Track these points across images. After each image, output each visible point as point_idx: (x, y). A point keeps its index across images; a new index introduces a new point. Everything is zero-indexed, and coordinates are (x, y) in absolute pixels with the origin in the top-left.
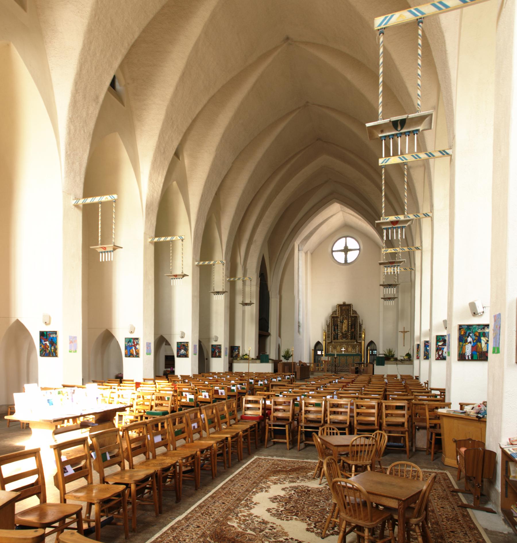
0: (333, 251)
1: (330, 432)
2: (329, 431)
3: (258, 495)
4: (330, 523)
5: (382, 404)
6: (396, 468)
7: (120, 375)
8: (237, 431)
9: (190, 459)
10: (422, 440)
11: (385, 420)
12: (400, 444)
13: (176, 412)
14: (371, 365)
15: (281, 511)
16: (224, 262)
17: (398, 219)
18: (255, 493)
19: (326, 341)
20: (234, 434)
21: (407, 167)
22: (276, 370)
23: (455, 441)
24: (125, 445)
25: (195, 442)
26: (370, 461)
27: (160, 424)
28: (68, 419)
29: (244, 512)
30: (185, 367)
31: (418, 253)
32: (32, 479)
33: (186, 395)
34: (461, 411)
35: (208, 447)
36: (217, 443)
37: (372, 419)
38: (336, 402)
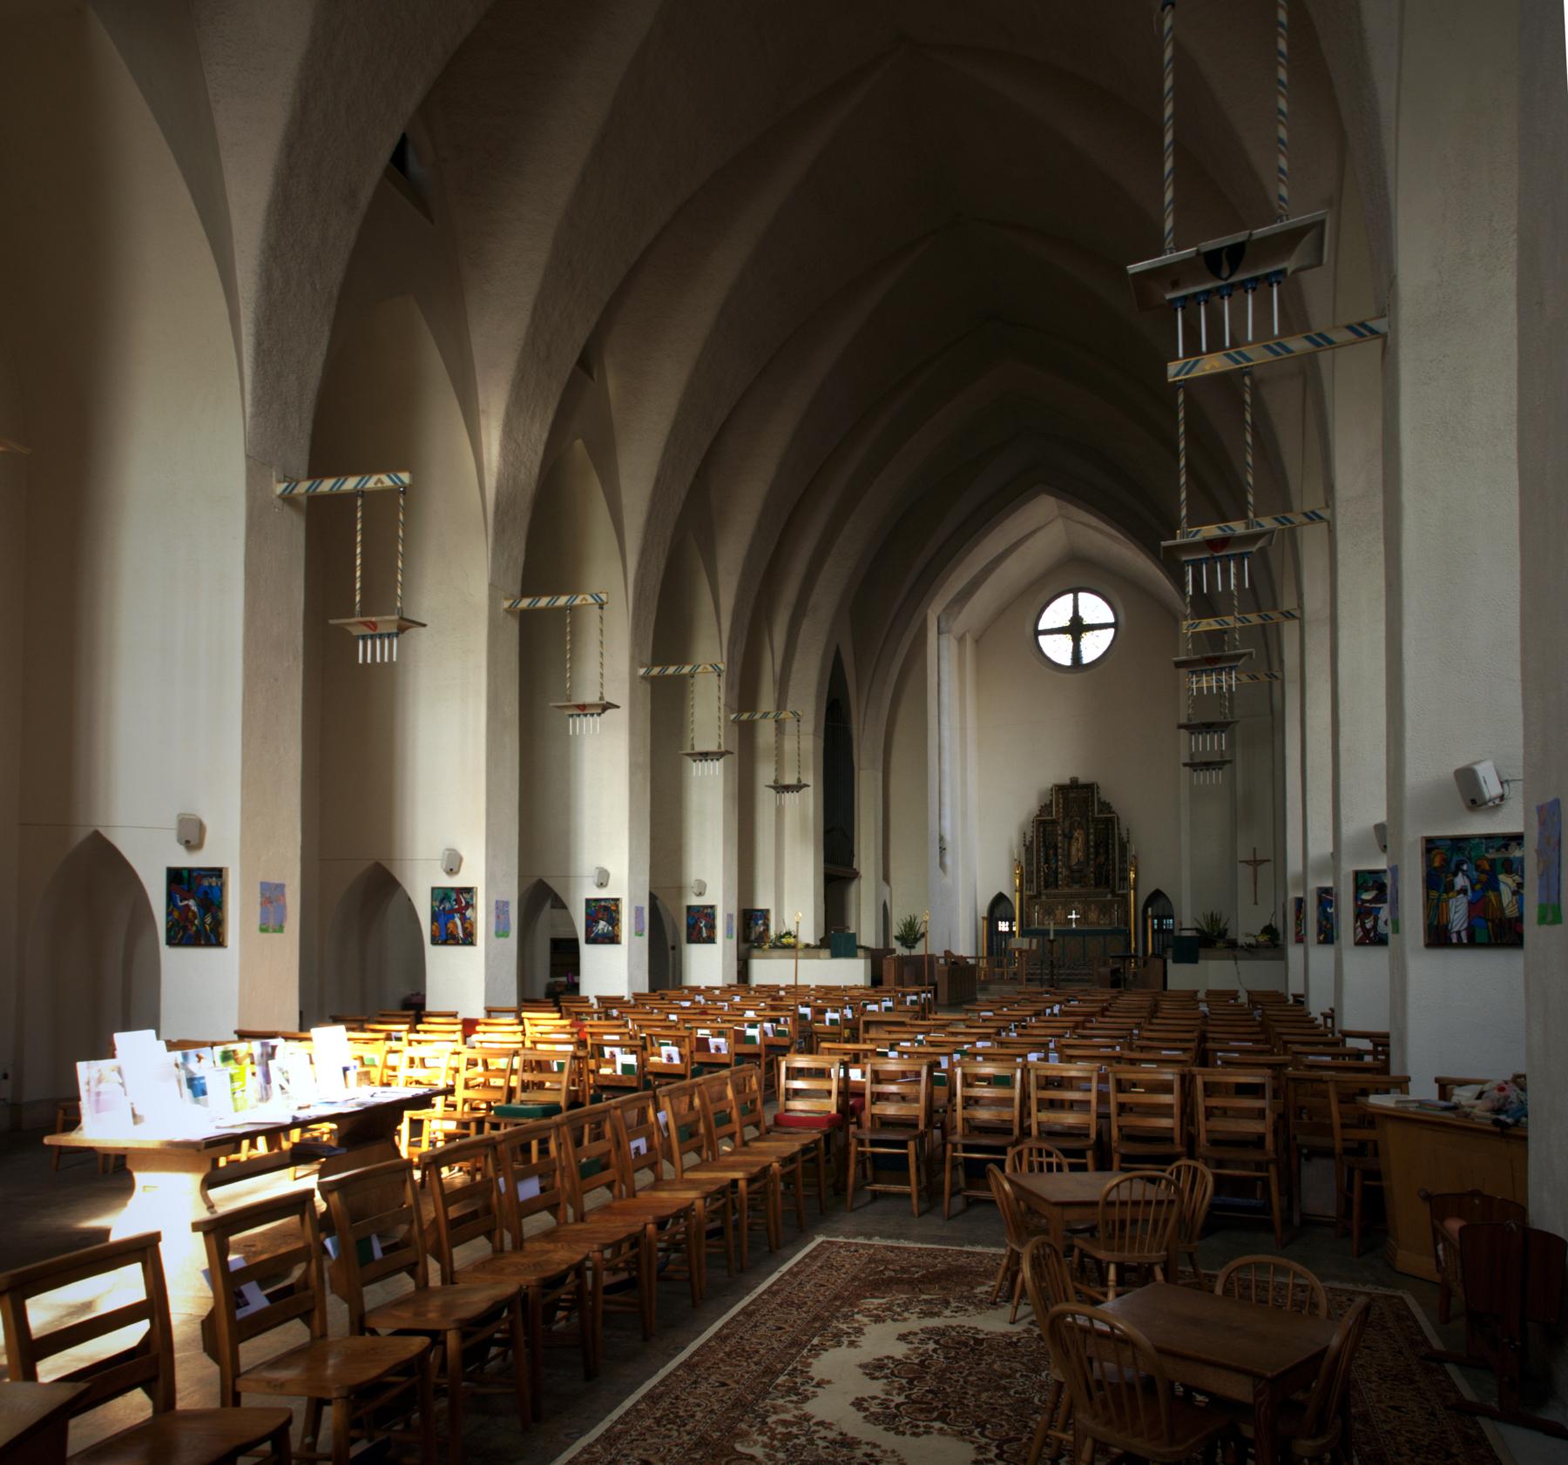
0: (1038, 633)
1: (1041, 1164)
2: (1035, 1159)
3: (826, 1357)
4: (1045, 1444)
5: (1193, 1077)
6: (1241, 1275)
7: (415, 1000)
8: (765, 1160)
9: (625, 1247)
10: (1320, 1189)
11: (1203, 1126)
12: (1254, 1202)
13: (582, 1105)
14: (1159, 963)
15: (898, 1406)
16: (722, 667)
17: (1229, 532)
18: (816, 1351)
19: (1021, 892)
20: (756, 1170)
21: (1252, 381)
22: (876, 980)
23: (1428, 1198)
24: (429, 1211)
25: (641, 1195)
26: (1163, 1253)
27: (534, 1144)
28: (252, 1136)
29: (786, 1411)
30: (610, 971)
31: (1290, 630)
32: (130, 1336)
33: (613, 1055)
34: (1443, 1103)
35: (679, 1211)
36: (705, 1198)
37: (1165, 1123)
38: (1055, 1073)
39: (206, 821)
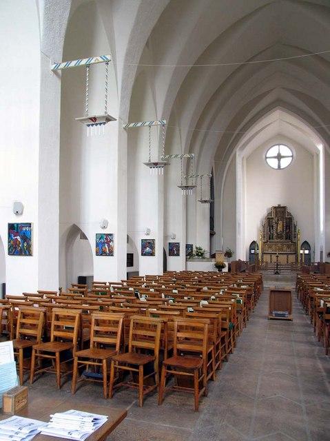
0: (266, 158)
39: (23, 203)
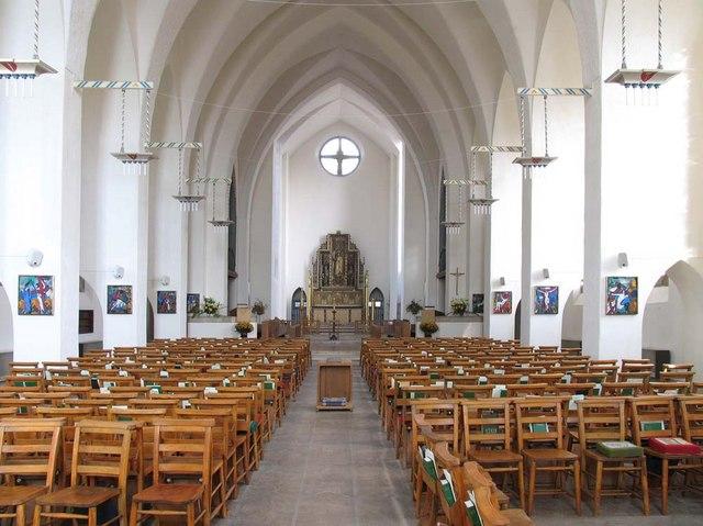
0: (321, 157)
